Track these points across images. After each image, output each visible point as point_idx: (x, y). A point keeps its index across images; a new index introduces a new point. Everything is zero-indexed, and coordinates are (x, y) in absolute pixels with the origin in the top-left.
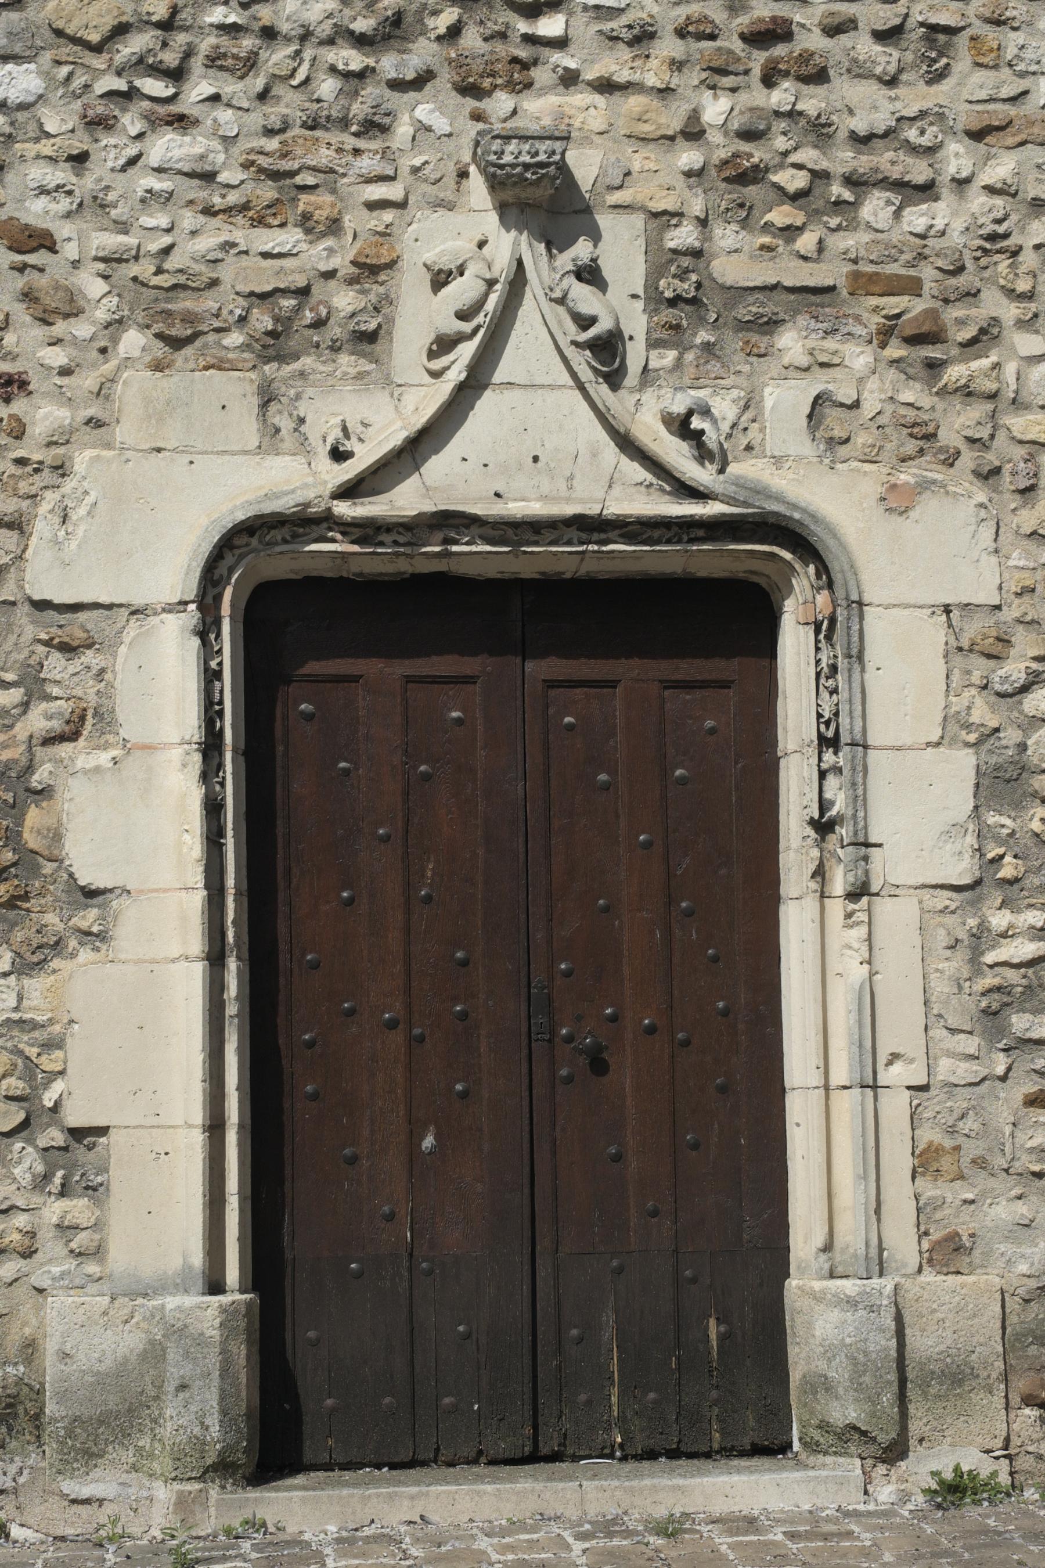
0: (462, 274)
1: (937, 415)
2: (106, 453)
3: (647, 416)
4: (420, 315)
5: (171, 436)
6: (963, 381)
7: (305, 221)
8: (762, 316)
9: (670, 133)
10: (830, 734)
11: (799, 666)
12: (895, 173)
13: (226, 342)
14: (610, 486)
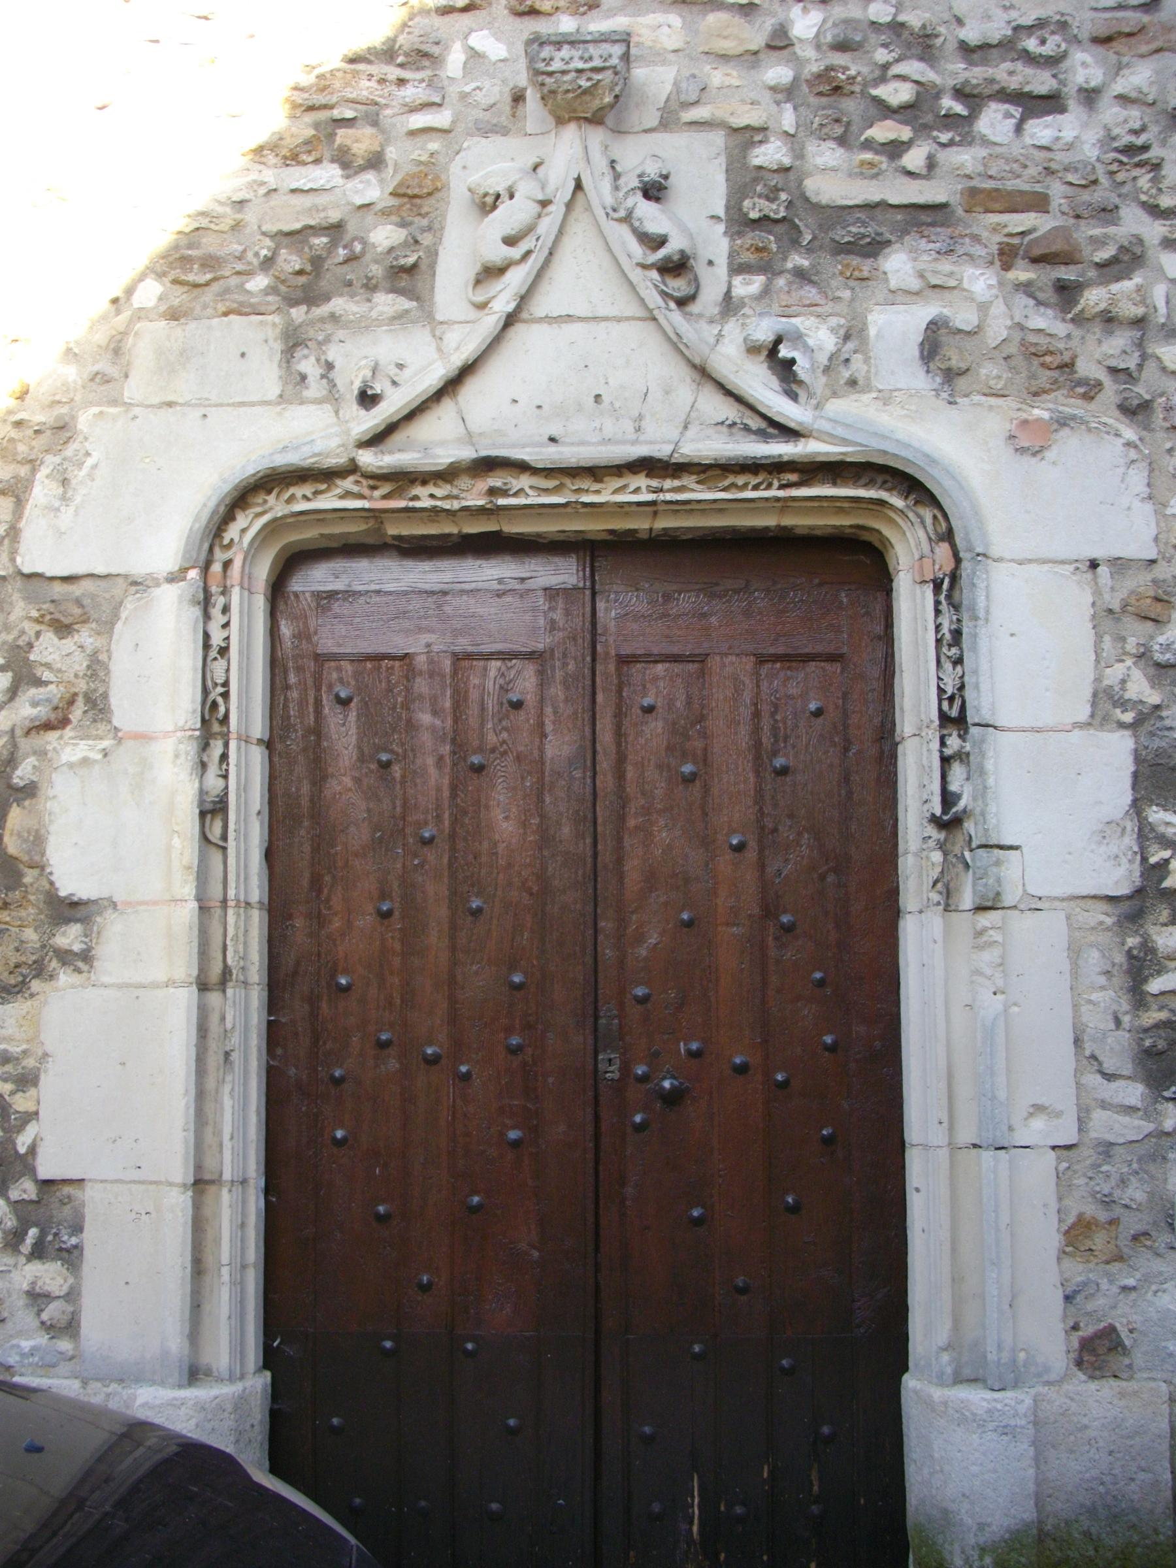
0: (512, 197)
1: (1074, 343)
2: (112, 410)
4: (463, 243)
6: (1103, 306)
7: (344, 160)
8: (864, 236)
9: (754, 47)
10: (954, 713)
11: (916, 630)
12: (1013, 84)
13: (248, 286)
14: (686, 427)
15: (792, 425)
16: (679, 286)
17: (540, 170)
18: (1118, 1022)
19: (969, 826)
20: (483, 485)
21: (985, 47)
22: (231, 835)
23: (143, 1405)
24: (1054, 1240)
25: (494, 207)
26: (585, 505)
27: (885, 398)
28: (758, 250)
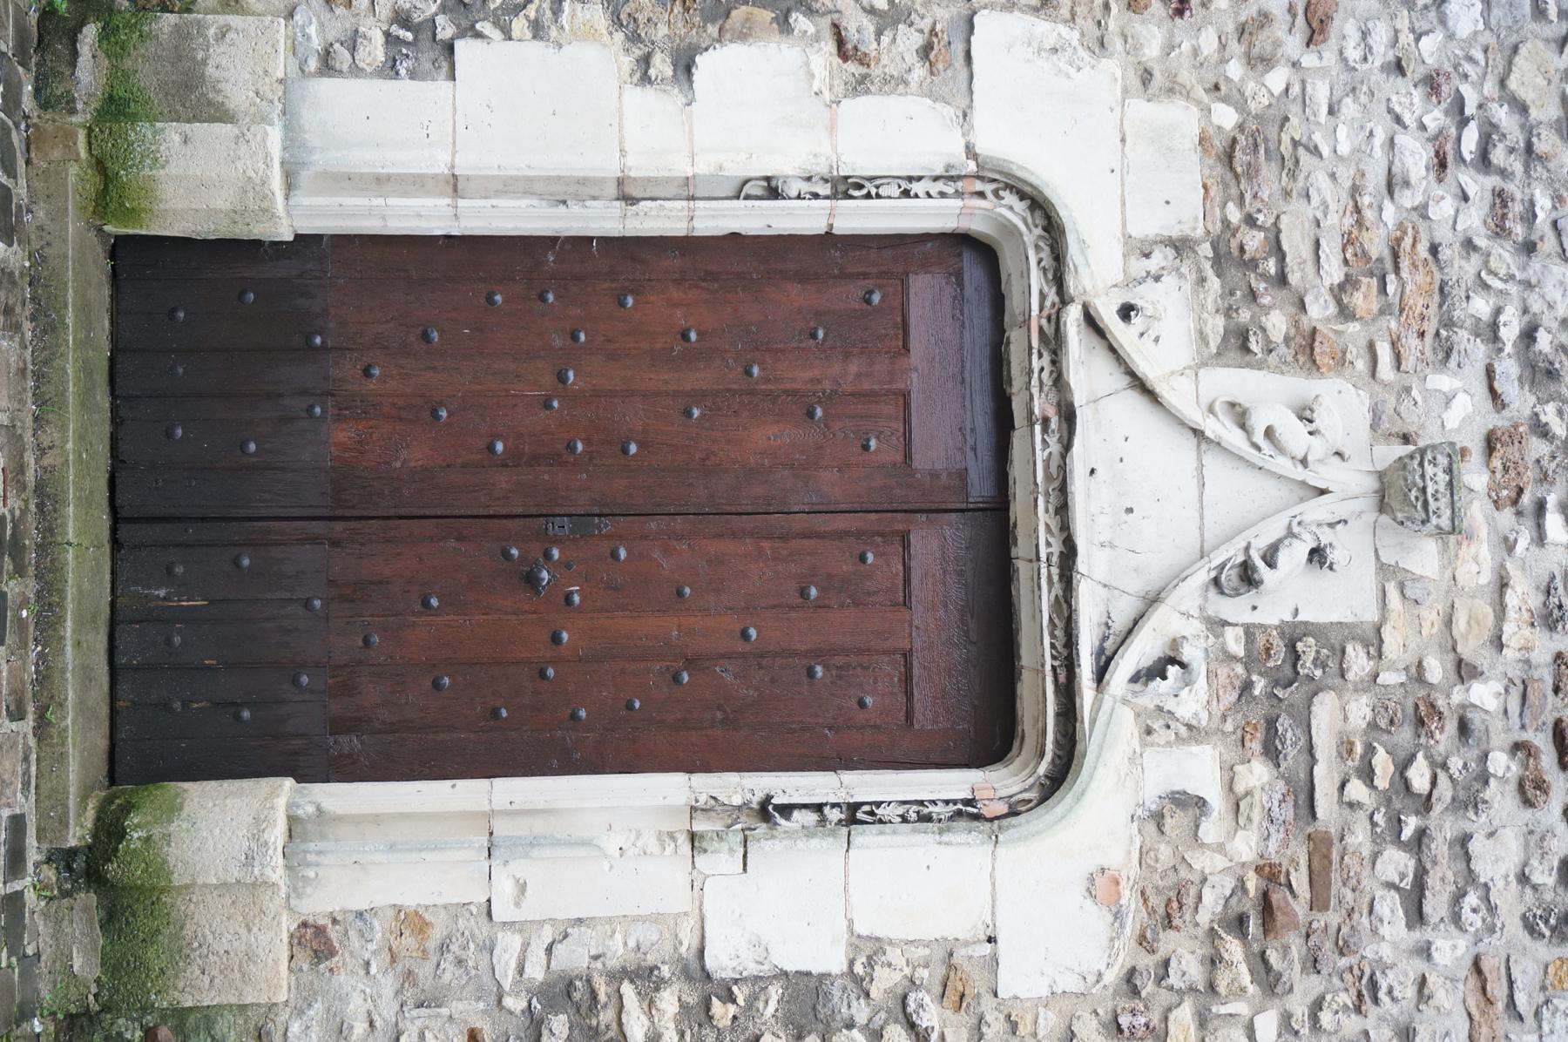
0: (1311, 433)
4: (1269, 391)
6: (1226, 956)
7: (1349, 284)
10: (860, 815)
12: (1432, 881)
13: (1231, 205)
15: (1107, 676)
16: (1230, 577)
17: (1337, 459)
18: (596, 958)
19: (762, 828)
20: (1051, 412)
21: (1468, 858)
22: (750, 203)
23: (266, 133)
24: (410, 900)
25: (1301, 418)
26: (1036, 500)
27: (1134, 759)
28: (1268, 650)
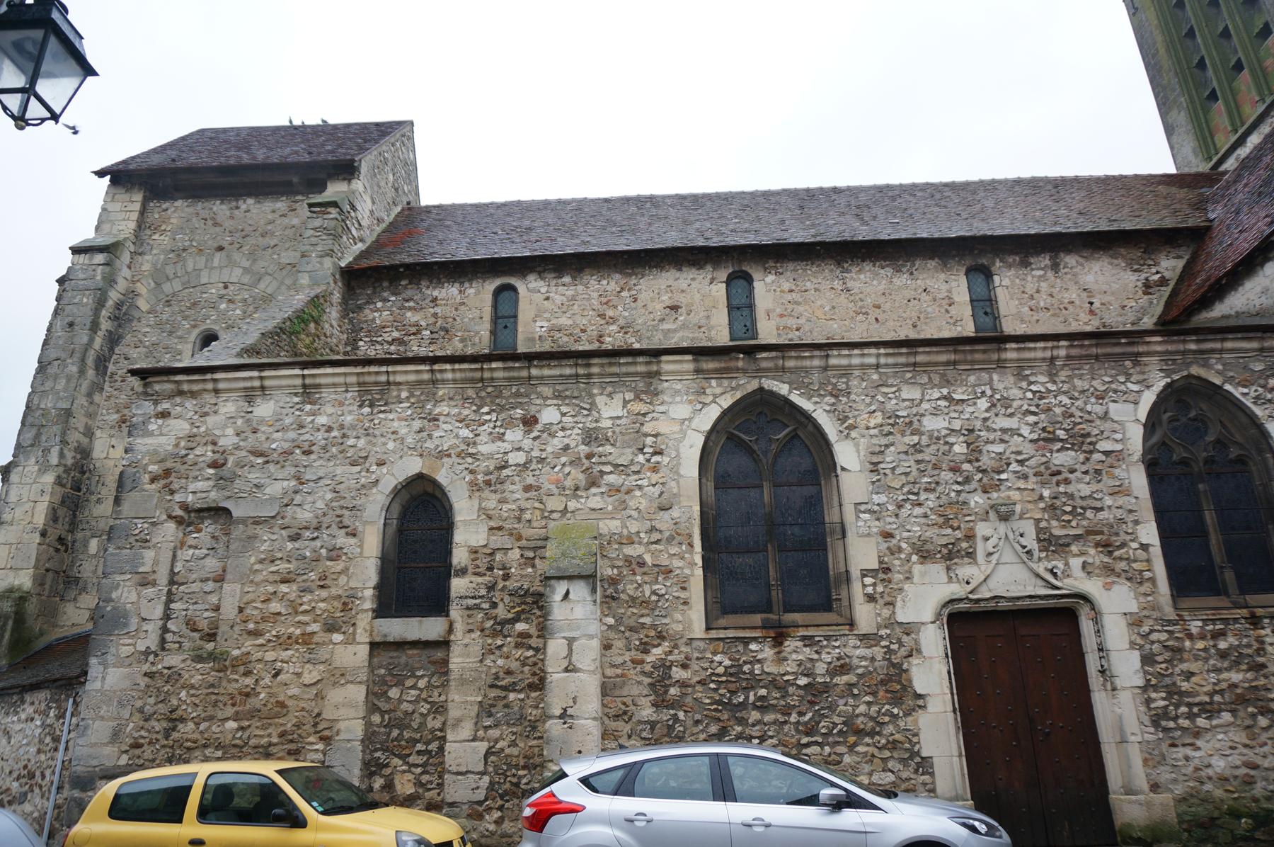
3: (1041, 569)
5: (927, 580)
7: (951, 527)
